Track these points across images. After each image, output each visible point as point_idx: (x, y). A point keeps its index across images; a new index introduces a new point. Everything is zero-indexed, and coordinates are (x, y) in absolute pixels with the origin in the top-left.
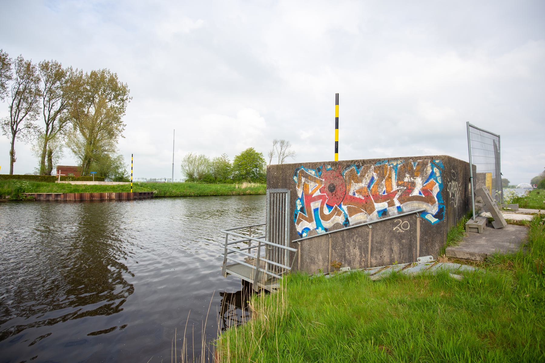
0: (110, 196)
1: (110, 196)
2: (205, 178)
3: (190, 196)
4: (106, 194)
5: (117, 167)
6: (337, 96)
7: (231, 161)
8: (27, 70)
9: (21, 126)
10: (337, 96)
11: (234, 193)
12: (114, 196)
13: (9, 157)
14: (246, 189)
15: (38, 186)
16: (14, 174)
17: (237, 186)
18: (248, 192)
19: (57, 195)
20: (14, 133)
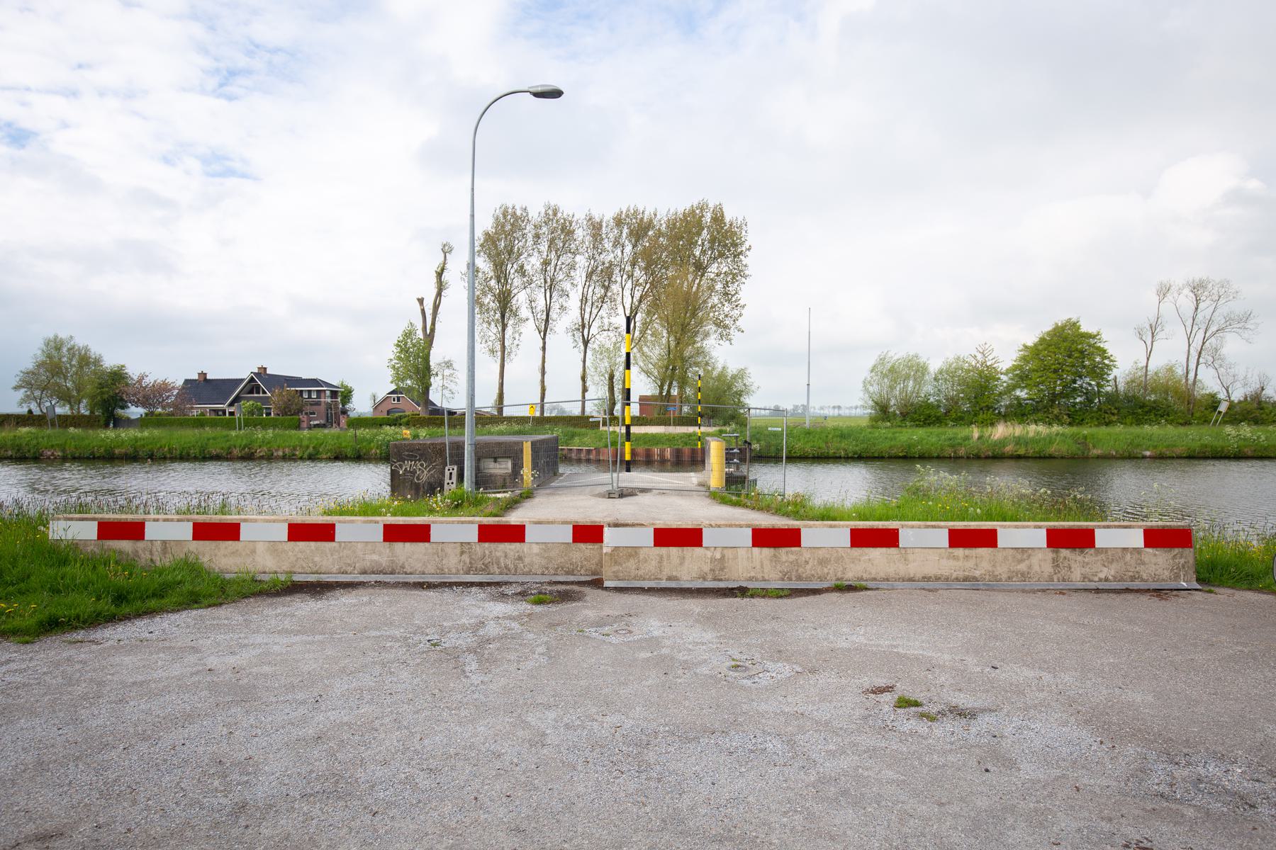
0: (662, 455)
1: (662, 455)
2: (922, 414)
3: (880, 458)
4: (656, 450)
5: (740, 394)
6: (556, 94)
7: (935, 366)
8: (596, 228)
9: (594, 330)
10: (556, 94)
11: (962, 452)
12: (668, 454)
13: (581, 382)
14: (1003, 442)
15: (573, 436)
16: (507, 412)
17: (976, 434)
18: (1009, 449)
19: (589, 452)
20: (586, 343)
